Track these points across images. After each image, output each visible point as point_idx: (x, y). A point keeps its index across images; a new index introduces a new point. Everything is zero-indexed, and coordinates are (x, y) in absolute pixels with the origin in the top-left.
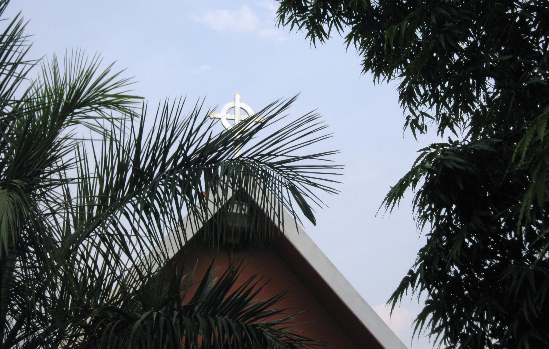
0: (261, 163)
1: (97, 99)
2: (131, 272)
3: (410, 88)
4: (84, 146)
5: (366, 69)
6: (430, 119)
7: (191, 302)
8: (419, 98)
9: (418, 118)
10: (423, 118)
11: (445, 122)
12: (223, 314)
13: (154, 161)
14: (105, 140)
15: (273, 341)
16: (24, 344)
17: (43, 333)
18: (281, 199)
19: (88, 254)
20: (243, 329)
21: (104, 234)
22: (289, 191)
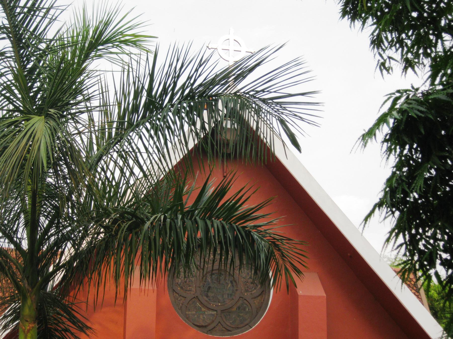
0: (255, 97)
1: (117, 38)
2: (142, 182)
3: (379, 35)
4: (106, 77)
5: (343, 16)
6: (396, 62)
7: (192, 207)
8: (386, 44)
9: (385, 61)
10: (390, 61)
11: (409, 64)
12: (218, 218)
13: (165, 91)
14: (124, 71)
15: (260, 240)
16: (55, 239)
17: (70, 230)
18: (272, 129)
19: (107, 167)
20: (235, 230)
21: (121, 152)
22: (278, 121)
